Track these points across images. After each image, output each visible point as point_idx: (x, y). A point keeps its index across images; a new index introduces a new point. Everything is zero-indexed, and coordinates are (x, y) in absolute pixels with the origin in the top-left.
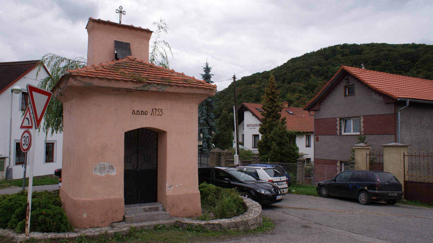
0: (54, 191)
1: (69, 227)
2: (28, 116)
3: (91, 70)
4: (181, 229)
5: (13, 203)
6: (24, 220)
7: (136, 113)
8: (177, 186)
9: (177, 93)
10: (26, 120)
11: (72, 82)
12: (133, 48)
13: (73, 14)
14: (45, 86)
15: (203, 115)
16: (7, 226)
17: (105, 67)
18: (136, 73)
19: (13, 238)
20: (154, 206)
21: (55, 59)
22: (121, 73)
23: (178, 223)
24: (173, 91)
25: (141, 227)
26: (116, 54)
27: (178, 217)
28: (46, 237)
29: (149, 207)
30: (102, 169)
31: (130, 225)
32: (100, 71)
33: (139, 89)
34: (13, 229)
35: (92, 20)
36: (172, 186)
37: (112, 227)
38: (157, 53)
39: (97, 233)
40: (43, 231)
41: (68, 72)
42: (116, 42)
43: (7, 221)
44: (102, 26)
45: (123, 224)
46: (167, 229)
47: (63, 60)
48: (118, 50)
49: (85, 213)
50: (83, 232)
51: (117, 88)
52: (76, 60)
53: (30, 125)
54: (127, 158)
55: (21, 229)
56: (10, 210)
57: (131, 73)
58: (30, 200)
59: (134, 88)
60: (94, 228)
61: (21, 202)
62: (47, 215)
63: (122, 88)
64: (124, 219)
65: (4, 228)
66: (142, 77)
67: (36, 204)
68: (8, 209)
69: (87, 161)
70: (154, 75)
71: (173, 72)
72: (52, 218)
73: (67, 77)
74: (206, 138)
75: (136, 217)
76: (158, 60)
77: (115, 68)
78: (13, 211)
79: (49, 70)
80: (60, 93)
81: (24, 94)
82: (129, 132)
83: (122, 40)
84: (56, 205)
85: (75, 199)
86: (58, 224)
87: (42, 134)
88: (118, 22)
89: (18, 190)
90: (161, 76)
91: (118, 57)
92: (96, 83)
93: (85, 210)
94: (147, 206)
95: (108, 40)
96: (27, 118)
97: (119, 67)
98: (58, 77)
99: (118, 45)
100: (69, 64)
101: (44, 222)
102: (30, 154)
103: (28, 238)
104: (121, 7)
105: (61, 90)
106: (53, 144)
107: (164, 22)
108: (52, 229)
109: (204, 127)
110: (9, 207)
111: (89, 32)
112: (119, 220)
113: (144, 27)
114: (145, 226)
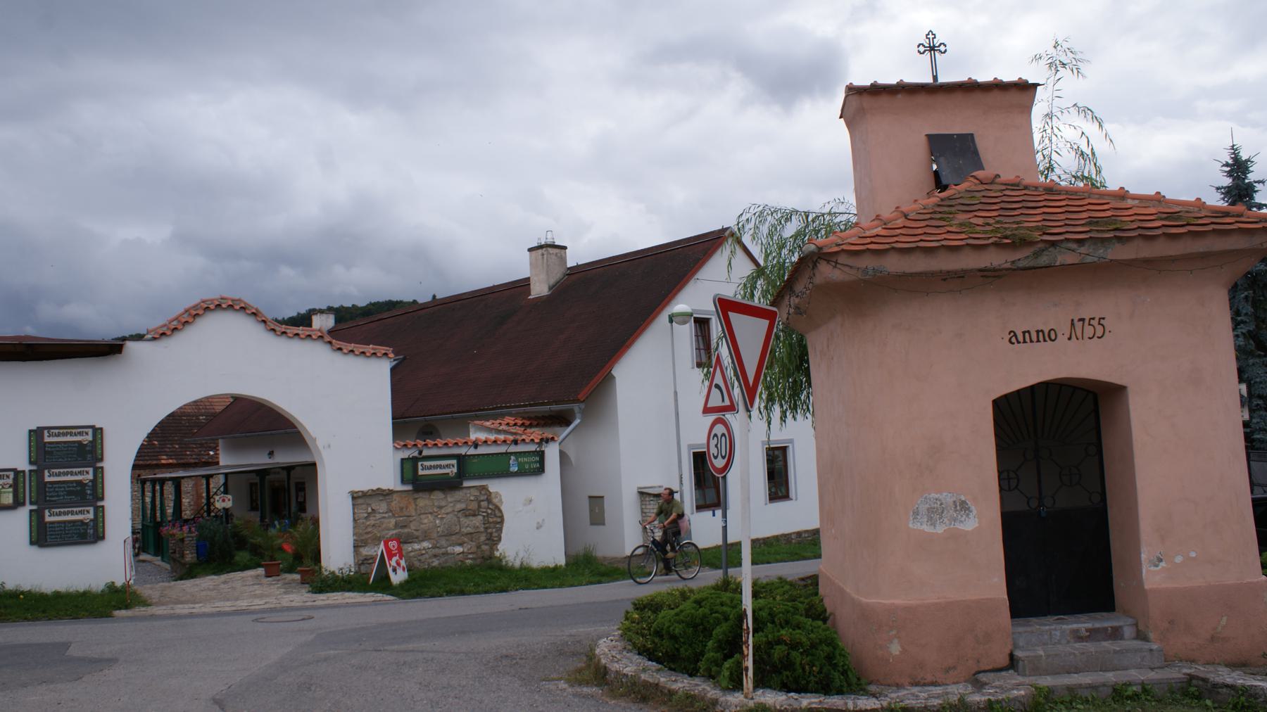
0: (803, 579)
1: (854, 680)
2: (718, 379)
3: (874, 232)
4: (1208, 702)
5: (707, 611)
6: (737, 656)
7: (1021, 339)
8: (1179, 559)
9: (1148, 262)
10: (714, 390)
11: (826, 272)
12: (984, 145)
13: (785, 81)
14: (752, 295)
15: (1242, 322)
16: (698, 671)
17: (912, 216)
18: (1008, 220)
19: (715, 702)
20: (1106, 624)
21: (769, 218)
22: (961, 225)
23: (1194, 682)
24: (1133, 256)
25: (1070, 689)
26: (936, 173)
27: (1193, 661)
28: (796, 705)
29: (1089, 625)
30: (935, 513)
31: (1032, 680)
32: (899, 231)
33: (1021, 264)
34: (713, 678)
35: (853, 91)
36: (1161, 560)
37: (979, 685)
38: (1061, 145)
39: (936, 702)
40: (786, 688)
41: (812, 247)
42: (931, 139)
43: (697, 657)
44: (884, 100)
45: (1011, 678)
46: (1159, 701)
47: (788, 216)
48: (942, 160)
49: (896, 641)
50: (893, 695)
51: (956, 272)
52: (826, 210)
53: (727, 402)
54: (1005, 475)
55: (731, 679)
56: (700, 627)
57: (991, 221)
58: (747, 603)
59: (1008, 265)
60: (924, 685)
61: (725, 608)
62: (794, 646)
63: (971, 270)
64: (1013, 663)
65: (691, 675)
66: (1028, 228)
67: (764, 614)
68: (695, 626)
69: (890, 489)
70: (1063, 217)
71: (1122, 195)
72: (806, 653)
73: (809, 261)
74: (1260, 397)
75: (1048, 656)
76: (1065, 168)
77: (941, 213)
78: (708, 633)
79: (756, 251)
80: (797, 307)
81: (702, 324)
82: (1006, 397)
83: (947, 131)
84: (813, 619)
85: (864, 600)
86: (825, 670)
87: (758, 423)
88: (929, 80)
89: (710, 577)
90: (1084, 215)
91: (944, 182)
92: (893, 264)
93: (894, 632)
94: (1083, 624)
95: (909, 136)
96: (717, 386)
97: (953, 209)
98: (782, 266)
99: (939, 145)
100: (807, 226)
101: (788, 664)
102: (733, 477)
103: (751, 704)
104: (931, 35)
105: (797, 300)
106: (784, 449)
107: (1065, 45)
108: (808, 682)
109: (1251, 361)
110: (698, 621)
111: (849, 125)
112: (1000, 666)
113: (1008, 76)
114: (1080, 686)
